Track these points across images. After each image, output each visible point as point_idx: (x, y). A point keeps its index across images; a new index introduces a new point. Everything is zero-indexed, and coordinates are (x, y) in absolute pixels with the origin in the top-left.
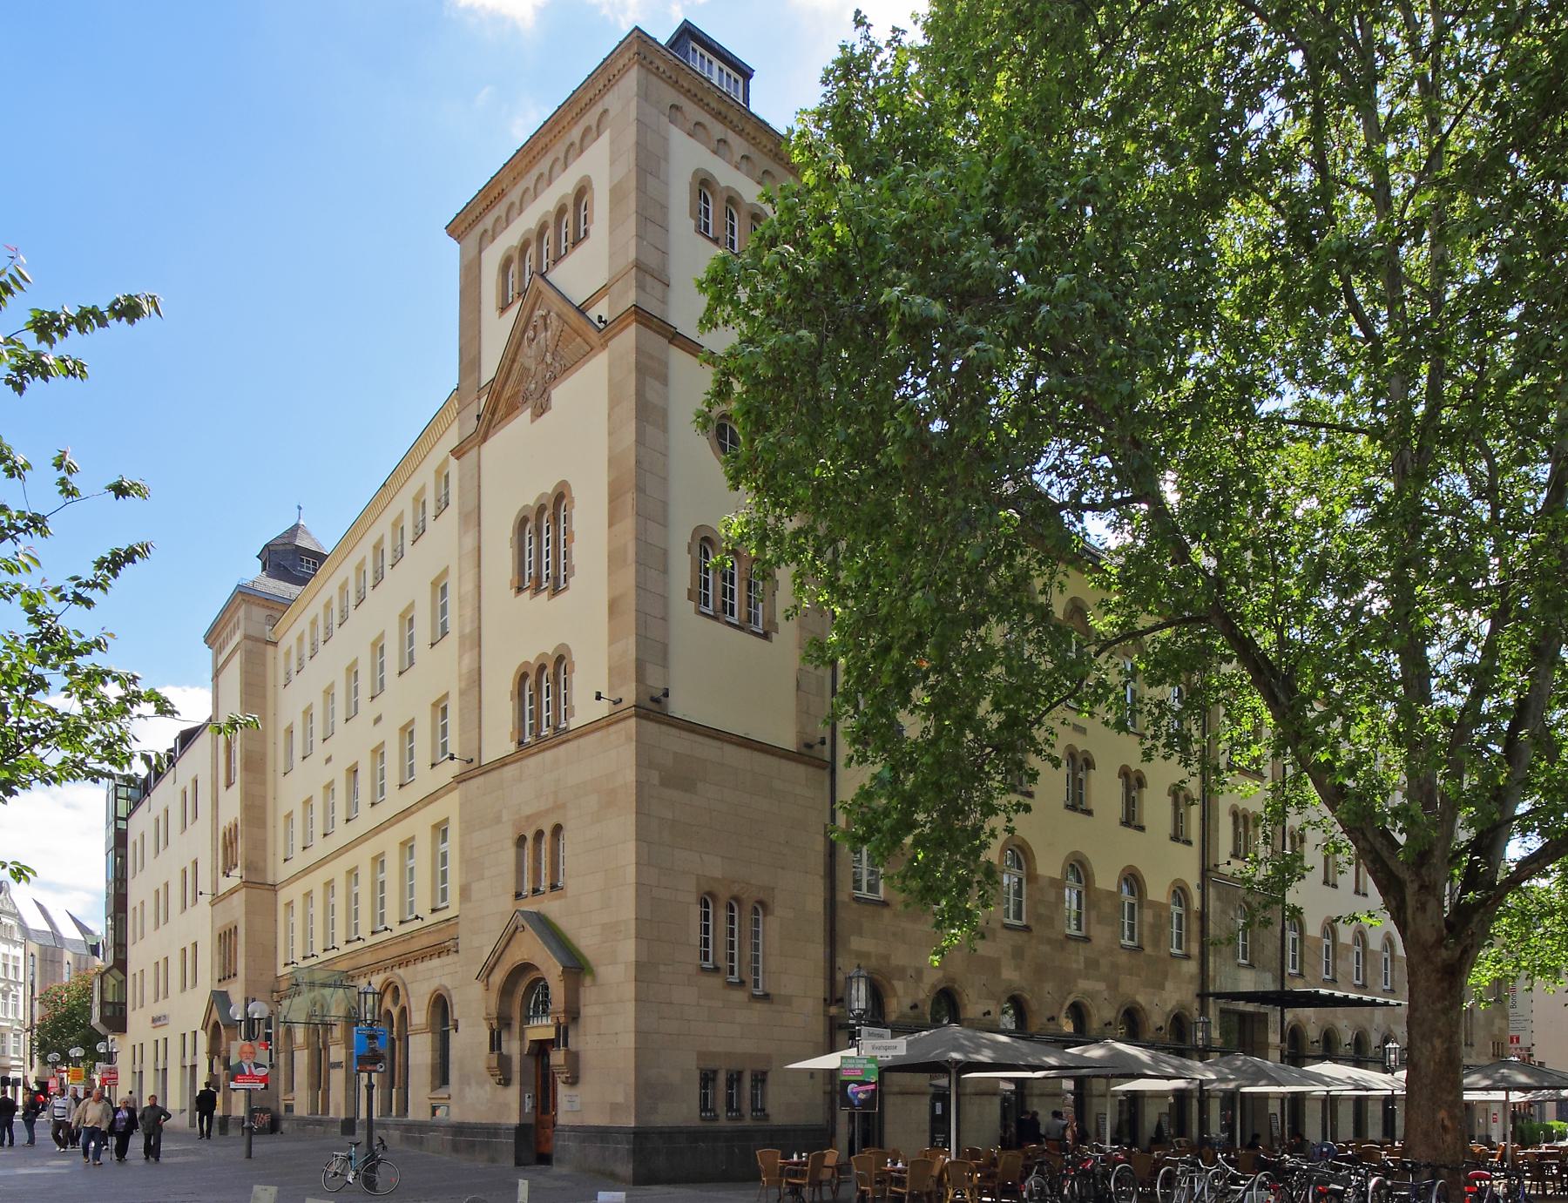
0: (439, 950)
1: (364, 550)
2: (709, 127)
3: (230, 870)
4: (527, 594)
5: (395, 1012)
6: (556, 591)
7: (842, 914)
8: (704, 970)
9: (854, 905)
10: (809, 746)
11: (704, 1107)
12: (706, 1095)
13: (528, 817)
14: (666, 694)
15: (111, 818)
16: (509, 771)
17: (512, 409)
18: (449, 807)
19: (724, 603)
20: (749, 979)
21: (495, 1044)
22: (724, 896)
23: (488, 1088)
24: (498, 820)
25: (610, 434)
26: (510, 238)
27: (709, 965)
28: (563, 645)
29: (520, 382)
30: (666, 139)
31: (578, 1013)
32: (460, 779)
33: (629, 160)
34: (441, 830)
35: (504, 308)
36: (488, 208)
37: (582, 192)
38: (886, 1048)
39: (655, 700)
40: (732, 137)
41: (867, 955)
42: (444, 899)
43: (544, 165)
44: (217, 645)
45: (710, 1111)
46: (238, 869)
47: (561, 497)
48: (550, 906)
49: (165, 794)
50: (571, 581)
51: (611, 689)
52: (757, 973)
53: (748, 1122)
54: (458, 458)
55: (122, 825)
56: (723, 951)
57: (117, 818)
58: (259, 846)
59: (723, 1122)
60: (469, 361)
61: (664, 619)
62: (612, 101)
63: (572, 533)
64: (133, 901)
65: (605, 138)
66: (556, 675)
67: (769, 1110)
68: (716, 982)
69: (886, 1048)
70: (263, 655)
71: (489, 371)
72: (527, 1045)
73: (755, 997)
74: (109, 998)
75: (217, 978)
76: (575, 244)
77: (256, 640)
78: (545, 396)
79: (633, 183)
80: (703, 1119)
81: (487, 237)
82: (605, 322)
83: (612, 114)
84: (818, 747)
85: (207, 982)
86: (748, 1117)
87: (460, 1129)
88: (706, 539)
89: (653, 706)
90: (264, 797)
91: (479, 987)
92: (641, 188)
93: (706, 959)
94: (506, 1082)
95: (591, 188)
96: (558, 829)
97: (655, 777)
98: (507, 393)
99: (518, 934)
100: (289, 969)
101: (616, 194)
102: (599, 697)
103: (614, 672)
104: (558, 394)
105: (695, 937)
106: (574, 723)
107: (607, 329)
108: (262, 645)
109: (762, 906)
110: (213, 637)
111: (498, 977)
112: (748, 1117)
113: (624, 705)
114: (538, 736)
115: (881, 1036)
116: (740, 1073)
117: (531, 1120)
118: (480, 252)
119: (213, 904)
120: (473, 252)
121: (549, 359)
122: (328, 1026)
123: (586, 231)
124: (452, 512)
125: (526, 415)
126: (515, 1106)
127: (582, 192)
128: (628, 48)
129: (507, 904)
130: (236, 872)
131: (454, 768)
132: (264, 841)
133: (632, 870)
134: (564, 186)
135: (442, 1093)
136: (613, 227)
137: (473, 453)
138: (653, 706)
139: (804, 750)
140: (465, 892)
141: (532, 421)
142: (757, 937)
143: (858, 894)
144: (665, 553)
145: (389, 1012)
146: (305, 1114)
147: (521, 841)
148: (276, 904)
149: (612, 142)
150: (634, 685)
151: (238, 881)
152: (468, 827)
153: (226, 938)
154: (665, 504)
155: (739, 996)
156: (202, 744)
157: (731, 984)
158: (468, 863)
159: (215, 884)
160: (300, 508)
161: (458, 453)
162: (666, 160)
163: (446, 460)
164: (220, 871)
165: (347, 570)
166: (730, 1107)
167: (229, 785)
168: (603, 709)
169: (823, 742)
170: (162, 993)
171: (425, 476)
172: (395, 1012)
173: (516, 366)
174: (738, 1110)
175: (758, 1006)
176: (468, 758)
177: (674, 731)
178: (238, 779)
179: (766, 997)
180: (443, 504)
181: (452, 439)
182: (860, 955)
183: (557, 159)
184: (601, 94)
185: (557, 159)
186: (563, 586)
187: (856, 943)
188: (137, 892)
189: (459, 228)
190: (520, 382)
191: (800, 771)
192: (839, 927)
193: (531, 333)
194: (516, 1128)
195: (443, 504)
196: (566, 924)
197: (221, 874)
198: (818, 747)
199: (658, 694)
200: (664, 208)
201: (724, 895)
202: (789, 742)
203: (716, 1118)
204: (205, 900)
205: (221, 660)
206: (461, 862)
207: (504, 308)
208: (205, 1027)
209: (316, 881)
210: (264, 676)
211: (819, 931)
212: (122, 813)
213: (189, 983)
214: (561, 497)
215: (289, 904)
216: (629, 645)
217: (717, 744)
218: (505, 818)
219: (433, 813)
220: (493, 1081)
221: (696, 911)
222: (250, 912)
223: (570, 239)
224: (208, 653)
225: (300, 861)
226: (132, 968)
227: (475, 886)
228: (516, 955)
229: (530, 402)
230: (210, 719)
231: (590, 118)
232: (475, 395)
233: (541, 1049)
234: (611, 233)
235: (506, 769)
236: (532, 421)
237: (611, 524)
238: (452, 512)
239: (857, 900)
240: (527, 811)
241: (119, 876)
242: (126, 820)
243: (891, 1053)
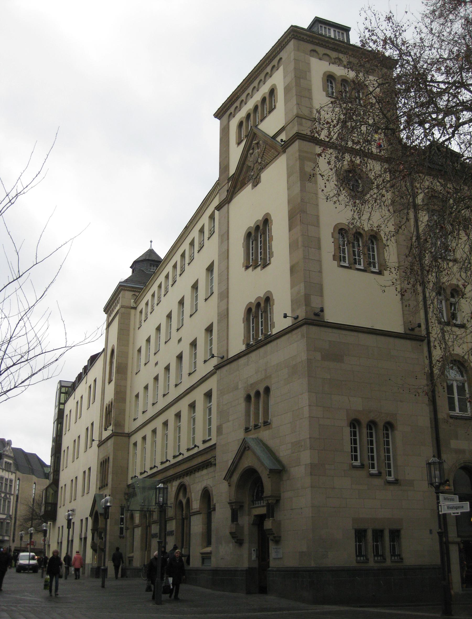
0: (208, 464)
1: (177, 258)
2: (329, 54)
3: (108, 427)
4: (259, 268)
5: (184, 502)
6: (265, 265)
7: (443, 427)
8: (355, 467)
9: (451, 421)
10: (413, 330)
11: (359, 553)
12: (360, 547)
13: (251, 385)
14: (322, 310)
15: (57, 404)
16: (242, 361)
17: (243, 185)
18: (212, 384)
19: (355, 259)
20: (384, 470)
21: (234, 518)
22: (364, 421)
23: (231, 545)
24: (236, 388)
25: (288, 189)
26: (242, 114)
27: (358, 463)
28: (269, 292)
29: (247, 172)
30: (309, 64)
31: (280, 497)
32: (218, 368)
33: (291, 76)
34: (208, 395)
35: (239, 144)
36: (232, 105)
37: (272, 92)
38: (457, 508)
39: (316, 315)
40: (341, 56)
41: (463, 451)
42: (210, 434)
43: (255, 84)
44: (109, 312)
45: (363, 556)
46: (112, 426)
47: (266, 221)
48: (264, 434)
49: (82, 390)
50: (272, 259)
51: (293, 310)
52: (389, 466)
53: (388, 563)
54: (218, 211)
55: (62, 407)
56: (366, 454)
57: (60, 403)
58: (122, 412)
59: (371, 564)
60: (224, 167)
61: (320, 272)
62: (283, 54)
63: (272, 236)
64: (64, 447)
65: (281, 69)
66: (266, 307)
67: (404, 556)
68: (363, 473)
69: (457, 508)
70: (129, 314)
71: (232, 170)
72: (253, 518)
73: (389, 483)
74: (50, 501)
75: (98, 486)
76: (270, 112)
77: (127, 307)
78: (258, 177)
79: (294, 84)
80: (358, 562)
81: (232, 115)
82: (284, 141)
83: (283, 60)
84: (417, 329)
85: (93, 490)
86: (371, 559)
87: (215, 572)
88: (341, 230)
89: (316, 318)
90: (126, 386)
91: (226, 483)
92: (298, 84)
93: (356, 460)
94: (239, 542)
95: (276, 89)
96: (267, 390)
97: (318, 356)
98: (241, 179)
99: (246, 452)
100: (134, 480)
101: (287, 90)
102: (285, 316)
103: (294, 302)
104: (265, 176)
105: (348, 447)
106: (275, 331)
107: (286, 145)
108: (129, 309)
109: (389, 426)
110: (108, 309)
111: (236, 477)
112: (371, 559)
113: (300, 319)
114: (257, 339)
115: (452, 500)
116: (382, 531)
117: (256, 565)
118: (229, 122)
119: (99, 446)
120: (225, 123)
121: (259, 161)
122: (151, 513)
123: (275, 106)
124: (216, 235)
125: (250, 186)
126: (246, 556)
127: (272, 92)
128: (289, 34)
129: (241, 434)
130: (111, 428)
131: (215, 361)
132: (124, 410)
133: (306, 409)
134: (264, 89)
135: (208, 550)
136: (286, 101)
137: (225, 208)
138: (316, 318)
139: (408, 332)
140: (219, 429)
141: (252, 189)
142: (388, 444)
143: (452, 413)
144: (319, 240)
145: (181, 503)
146: (139, 566)
147: (248, 398)
148: (129, 444)
149: (284, 69)
150: (304, 307)
151: (111, 432)
152: (221, 393)
153: (104, 464)
154: (318, 217)
155: (377, 482)
156: (99, 363)
157: (372, 475)
158: (221, 413)
159: (101, 434)
160: (151, 242)
161: (218, 208)
162: (310, 71)
163: (214, 212)
164: (103, 427)
165: (169, 268)
166: (377, 555)
167: (109, 383)
168: (288, 322)
169: (419, 326)
170: (74, 498)
171: (205, 220)
172: (184, 502)
173: (245, 166)
174: (366, 556)
175: (392, 487)
176: (221, 356)
177: (330, 330)
178: (114, 378)
179: (396, 482)
180: (212, 233)
181: (216, 202)
182: (459, 451)
183: (261, 80)
184: (279, 53)
185: (261, 80)
186: (268, 262)
187: (454, 444)
188: (67, 441)
189: (219, 114)
190: (247, 172)
191: (408, 344)
192: (441, 436)
193: (251, 151)
194: (246, 570)
195: (212, 233)
196: (271, 443)
197: (103, 429)
198: (417, 329)
199: (318, 311)
200: (309, 90)
201: (364, 421)
202: (400, 329)
203: (367, 561)
204: (95, 443)
205: (111, 319)
206: (217, 413)
207: (239, 144)
208: (91, 515)
209: (147, 431)
210: (129, 325)
211: (428, 437)
212: (62, 401)
213: (86, 492)
214: (266, 221)
215: (135, 444)
216: (301, 287)
217: (355, 334)
218: (240, 387)
219: (204, 388)
220: (234, 541)
221: (347, 430)
222: (116, 449)
223: (268, 110)
224: (105, 316)
225: (142, 419)
226: (61, 484)
227: (224, 426)
228: (247, 462)
229: (251, 181)
230: (104, 350)
231: (275, 62)
232: (227, 181)
233: (260, 520)
234: (285, 105)
235: (240, 360)
236: (252, 189)
237: (290, 230)
238: (216, 235)
239: (452, 417)
240: (251, 381)
241: (59, 434)
242: (64, 404)
243: (460, 511)
